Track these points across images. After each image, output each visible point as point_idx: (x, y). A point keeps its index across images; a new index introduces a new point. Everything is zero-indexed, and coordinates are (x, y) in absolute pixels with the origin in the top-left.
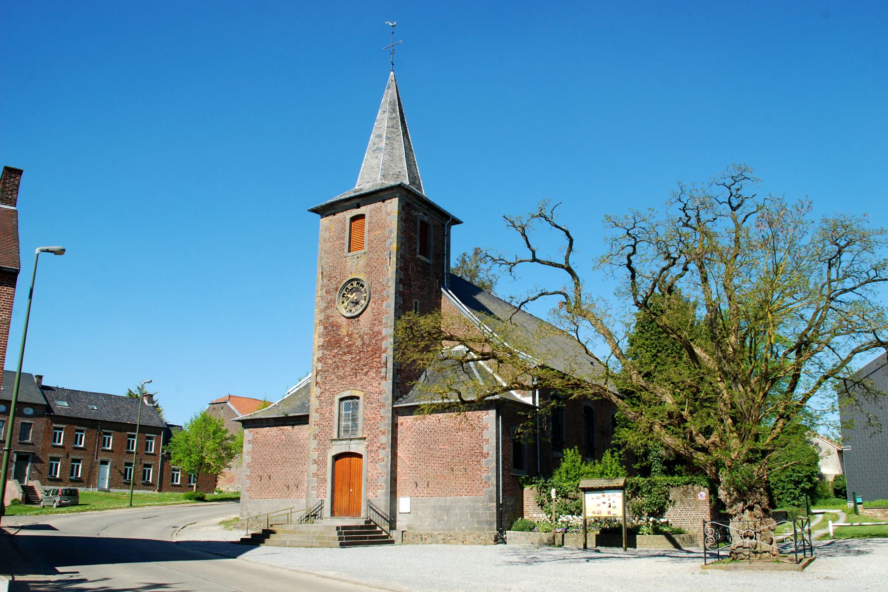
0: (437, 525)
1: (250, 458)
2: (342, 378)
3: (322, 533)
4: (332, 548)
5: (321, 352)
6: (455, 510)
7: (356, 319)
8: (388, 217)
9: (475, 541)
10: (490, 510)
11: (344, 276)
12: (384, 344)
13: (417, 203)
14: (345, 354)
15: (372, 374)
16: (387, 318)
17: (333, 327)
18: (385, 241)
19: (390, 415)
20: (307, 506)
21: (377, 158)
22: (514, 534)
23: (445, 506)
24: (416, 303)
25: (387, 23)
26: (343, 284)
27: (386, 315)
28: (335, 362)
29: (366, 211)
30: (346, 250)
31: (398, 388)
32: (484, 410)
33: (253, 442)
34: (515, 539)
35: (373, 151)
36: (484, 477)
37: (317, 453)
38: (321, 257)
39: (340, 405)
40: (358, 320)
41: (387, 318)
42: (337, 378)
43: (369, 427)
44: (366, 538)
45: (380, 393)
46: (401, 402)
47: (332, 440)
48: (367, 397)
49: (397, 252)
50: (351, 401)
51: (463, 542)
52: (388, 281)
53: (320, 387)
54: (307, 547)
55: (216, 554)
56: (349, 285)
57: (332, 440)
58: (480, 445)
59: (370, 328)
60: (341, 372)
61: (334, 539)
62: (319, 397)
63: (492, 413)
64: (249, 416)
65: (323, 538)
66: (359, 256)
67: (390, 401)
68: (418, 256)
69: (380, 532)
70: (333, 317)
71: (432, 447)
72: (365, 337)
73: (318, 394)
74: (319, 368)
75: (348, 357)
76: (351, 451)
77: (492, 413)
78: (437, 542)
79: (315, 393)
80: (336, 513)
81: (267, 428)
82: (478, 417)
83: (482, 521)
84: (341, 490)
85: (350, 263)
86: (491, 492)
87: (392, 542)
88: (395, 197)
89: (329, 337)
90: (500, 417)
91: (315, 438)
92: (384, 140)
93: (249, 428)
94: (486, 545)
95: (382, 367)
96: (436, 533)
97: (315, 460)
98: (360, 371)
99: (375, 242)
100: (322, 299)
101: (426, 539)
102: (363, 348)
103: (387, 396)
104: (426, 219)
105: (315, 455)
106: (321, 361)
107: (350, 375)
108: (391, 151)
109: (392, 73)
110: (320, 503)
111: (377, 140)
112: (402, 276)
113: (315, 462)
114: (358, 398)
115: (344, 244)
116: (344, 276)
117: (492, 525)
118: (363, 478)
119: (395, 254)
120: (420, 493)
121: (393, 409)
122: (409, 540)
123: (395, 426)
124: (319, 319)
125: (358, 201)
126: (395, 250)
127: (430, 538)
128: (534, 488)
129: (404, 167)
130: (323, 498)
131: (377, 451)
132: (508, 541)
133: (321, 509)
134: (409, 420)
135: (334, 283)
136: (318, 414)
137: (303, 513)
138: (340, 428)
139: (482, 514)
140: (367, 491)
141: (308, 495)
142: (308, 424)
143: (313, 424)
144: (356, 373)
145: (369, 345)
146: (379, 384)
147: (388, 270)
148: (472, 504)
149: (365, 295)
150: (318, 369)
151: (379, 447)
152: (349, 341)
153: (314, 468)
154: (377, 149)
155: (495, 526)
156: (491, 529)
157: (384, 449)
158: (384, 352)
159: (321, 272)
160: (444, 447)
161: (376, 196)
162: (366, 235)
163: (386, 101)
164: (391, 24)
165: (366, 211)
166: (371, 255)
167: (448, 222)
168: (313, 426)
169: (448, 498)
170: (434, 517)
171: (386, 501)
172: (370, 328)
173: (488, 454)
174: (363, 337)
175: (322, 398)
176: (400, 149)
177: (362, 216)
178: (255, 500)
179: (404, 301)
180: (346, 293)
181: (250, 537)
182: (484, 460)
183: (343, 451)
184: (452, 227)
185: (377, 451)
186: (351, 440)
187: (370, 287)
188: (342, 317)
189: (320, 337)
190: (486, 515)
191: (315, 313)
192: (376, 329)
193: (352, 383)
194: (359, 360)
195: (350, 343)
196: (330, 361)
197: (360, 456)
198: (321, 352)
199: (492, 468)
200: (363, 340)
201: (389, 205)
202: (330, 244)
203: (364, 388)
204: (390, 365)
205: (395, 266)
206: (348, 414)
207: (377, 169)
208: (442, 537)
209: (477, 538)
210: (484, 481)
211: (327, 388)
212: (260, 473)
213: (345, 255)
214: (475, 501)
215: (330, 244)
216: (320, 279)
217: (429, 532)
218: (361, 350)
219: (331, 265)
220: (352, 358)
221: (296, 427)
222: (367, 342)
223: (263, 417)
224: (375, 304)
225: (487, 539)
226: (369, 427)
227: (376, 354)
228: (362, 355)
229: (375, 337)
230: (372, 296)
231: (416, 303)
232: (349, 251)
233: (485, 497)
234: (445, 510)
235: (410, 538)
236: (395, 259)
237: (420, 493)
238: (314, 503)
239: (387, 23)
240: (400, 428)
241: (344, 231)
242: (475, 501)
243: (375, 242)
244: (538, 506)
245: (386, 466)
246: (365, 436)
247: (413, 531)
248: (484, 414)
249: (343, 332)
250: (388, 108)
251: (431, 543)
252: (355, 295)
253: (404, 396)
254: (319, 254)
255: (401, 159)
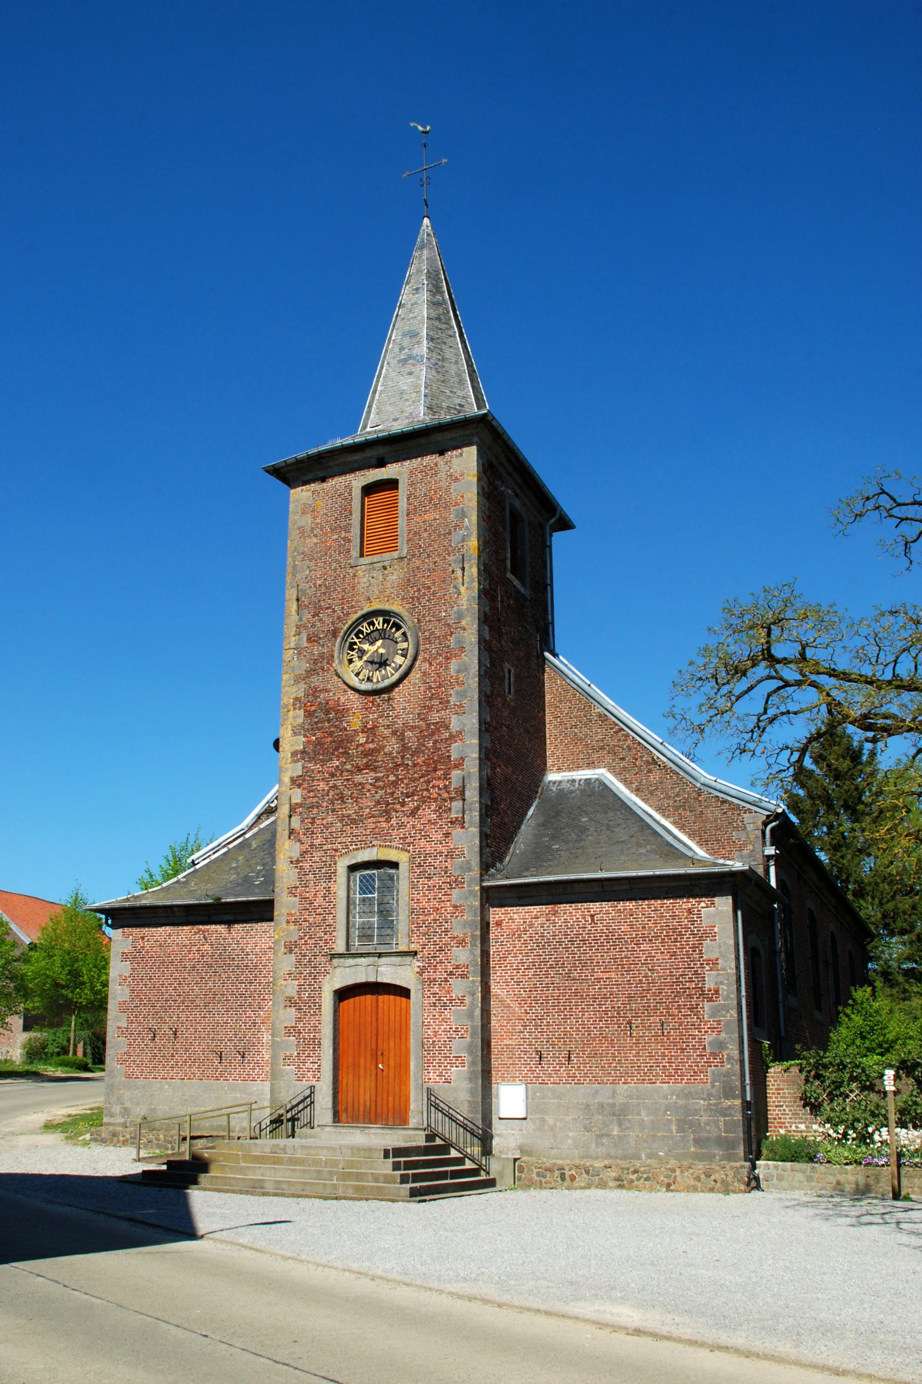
0: (593, 1146)
1: (127, 991)
2: (354, 821)
3: (351, 1164)
4: (393, 1201)
5: (299, 765)
6: (639, 1114)
7: (386, 696)
8: (454, 486)
9: (699, 1184)
10: (726, 1115)
11: (353, 607)
12: (455, 750)
13: (505, 468)
14: (360, 770)
15: (428, 813)
16: (462, 695)
17: (327, 712)
18: (450, 533)
19: (477, 903)
20: (273, 1099)
21: (410, 374)
22: (776, 1167)
23: (613, 1105)
24: (509, 671)
25: (412, 124)
26: (350, 622)
27: (457, 688)
28: (335, 786)
29: (399, 473)
30: (355, 553)
31: (488, 846)
32: (702, 896)
33: (134, 957)
34: (780, 1178)
35: (399, 361)
36: (710, 1043)
37: (297, 982)
38: (295, 566)
39: (349, 881)
40: (389, 699)
41: (462, 695)
42: (341, 821)
43: (423, 929)
44: (443, 1175)
45: (450, 855)
46: (493, 877)
47: (333, 956)
48: (419, 865)
49: (479, 556)
50: (375, 871)
51: (668, 1186)
52: (460, 616)
53: (299, 841)
54: (325, 1199)
55: (167, 1229)
56: (365, 624)
57: (333, 956)
58: (696, 973)
59: (419, 714)
60: (350, 810)
61: (388, 1179)
62: (298, 861)
63: (724, 904)
64: (125, 901)
65: (359, 1177)
66: (386, 564)
67: (476, 872)
68: (509, 576)
69: (460, 1161)
70: (327, 691)
71: (575, 974)
72: (408, 734)
73: (296, 855)
74: (297, 799)
75: (367, 777)
76: (379, 980)
77: (724, 904)
78: (603, 1185)
79: (288, 854)
80: (344, 1117)
81: (168, 928)
82: (690, 911)
83: (708, 1139)
84: (356, 1066)
85: (365, 580)
86: (727, 1074)
87: (490, 1183)
88: (469, 444)
89: (319, 735)
90: (739, 913)
91: (291, 951)
92: (425, 342)
93: (123, 927)
94: (727, 1192)
95: (451, 799)
96: (598, 1164)
97: (290, 999)
98: (398, 807)
99: (425, 535)
100: (299, 654)
101: (573, 1178)
102: (403, 757)
103: (468, 862)
104: (517, 504)
105: (291, 988)
106: (299, 786)
107: (373, 816)
108: (440, 363)
109: (426, 221)
110: (308, 1092)
111: (406, 342)
112: (487, 609)
113: (291, 1002)
114: (395, 865)
115: (350, 541)
116: (353, 607)
117: (734, 1148)
118: (412, 1041)
119: (475, 561)
120: (550, 1075)
121: (483, 889)
122: (531, 1180)
123: (485, 927)
124: (294, 696)
125: (380, 451)
126: (475, 553)
127: (584, 1175)
128: (791, 1069)
129: (469, 396)
130: (314, 1083)
131: (446, 980)
132: (763, 1184)
133: (310, 1105)
134: (516, 916)
135: (328, 620)
136: (297, 899)
137: (265, 1115)
138: (351, 930)
139: (707, 1123)
140: (425, 1065)
141: (274, 1075)
142: (271, 920)
143: (283, 920)
144: (387, 812)
145: (416, 753)
146: (447, 835)
147: (459, 594)
148: (680, 1102)
149: (405, 645)
150: (294, 801)
151: (451, 973)
152: (367, 742)
153: (289, 1016)
154: (410, 357)
155: (741, 1150)
156: (730, 1158)
157: (463, 976)
158: (456, 766)
159: (295, 597)
160: (607, 975)
161: (423, 440)
162: (402, 522)
163: (419, 271)
164: (420, 128)
165: (399, 473)
166: (417, 562)
167: (553, 520)
168: (284, 925)
169: (621, 1088)
170: (587, 1129)
171: (472, 1092)
172: (419, 714)
173: (717, 991)
174: (403, 734)
175: (306, 865)
176: (456, 363)
177: (391, 484)
178: (140, 1082)
179: (493, 664)
180: (356, 640)
181: (165, 1167)
182: (707, 1005)
183: (361, 979)
184: (554, 534)
185: (446, 980)
186: (380, 955)
187: (418, 627)
188: (350, 692)
189: (295, 734)
190: (717, 1127)
191: (283, 683)
192: (435, 717)
193: (377, 833)
194: (394, 784)
195: (371, 746)
196: (322, 785)
197: (404, 992)
198: (299, 765)
199: (729, 1023)
200: (403, 740)
201: (455, 461)
202: (315, 540)
203: (409, 844)
204: (472, 794)
205: (476, 584)
206: (370, 899)
207: (414, 395)
208: (614, 1174)
209: (703, 1176)
210: (708, 1050)
211: (317, 842)
212: (152, 1023)
213: (352, 562)
214: (688, 1096)
215: (315, 540)
216: (294, 613)
217: (577, 1162)
218: (399, 761)
219: (319, 582)
220: (377, 779)
221: (238, 926)
222: (413, 744)
223: (160, 903)
224: (430, 664)
225: (729, 1179)
226: (423, 929)
227: (435, 770)
228: (401, 772)
229: (433, 734)
230: (422, 647)
231: (509, 671)
232: (362, 555)
233: (713, 1086)
234: (614, 1115)
235: (534, 1175)
236: (475, 570)
237: (550, 1075)
238: (291, 1091)
239: (412, 124)
240: (494, 932)
241: (347, 513)
242: (688, 1096)
243: (425, 535)
244: (804, 1106)
245: (471, 1015)
246: (413, 947)
247: (534, 1159)
248: (703, 904)
249: (355, 722)
250: (425, 282)
251: (588, 1187)
252: (382, 646)
253: (498, 865)
254: (290, 559)
255: (461, 382)
